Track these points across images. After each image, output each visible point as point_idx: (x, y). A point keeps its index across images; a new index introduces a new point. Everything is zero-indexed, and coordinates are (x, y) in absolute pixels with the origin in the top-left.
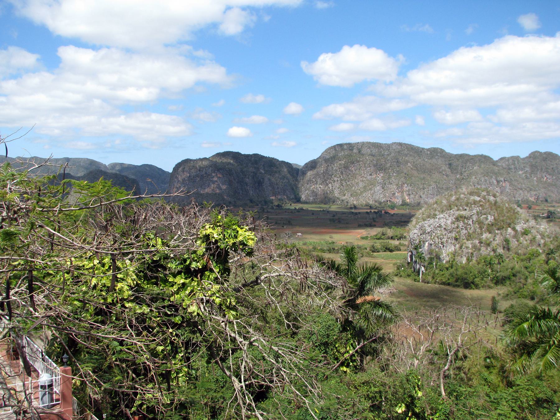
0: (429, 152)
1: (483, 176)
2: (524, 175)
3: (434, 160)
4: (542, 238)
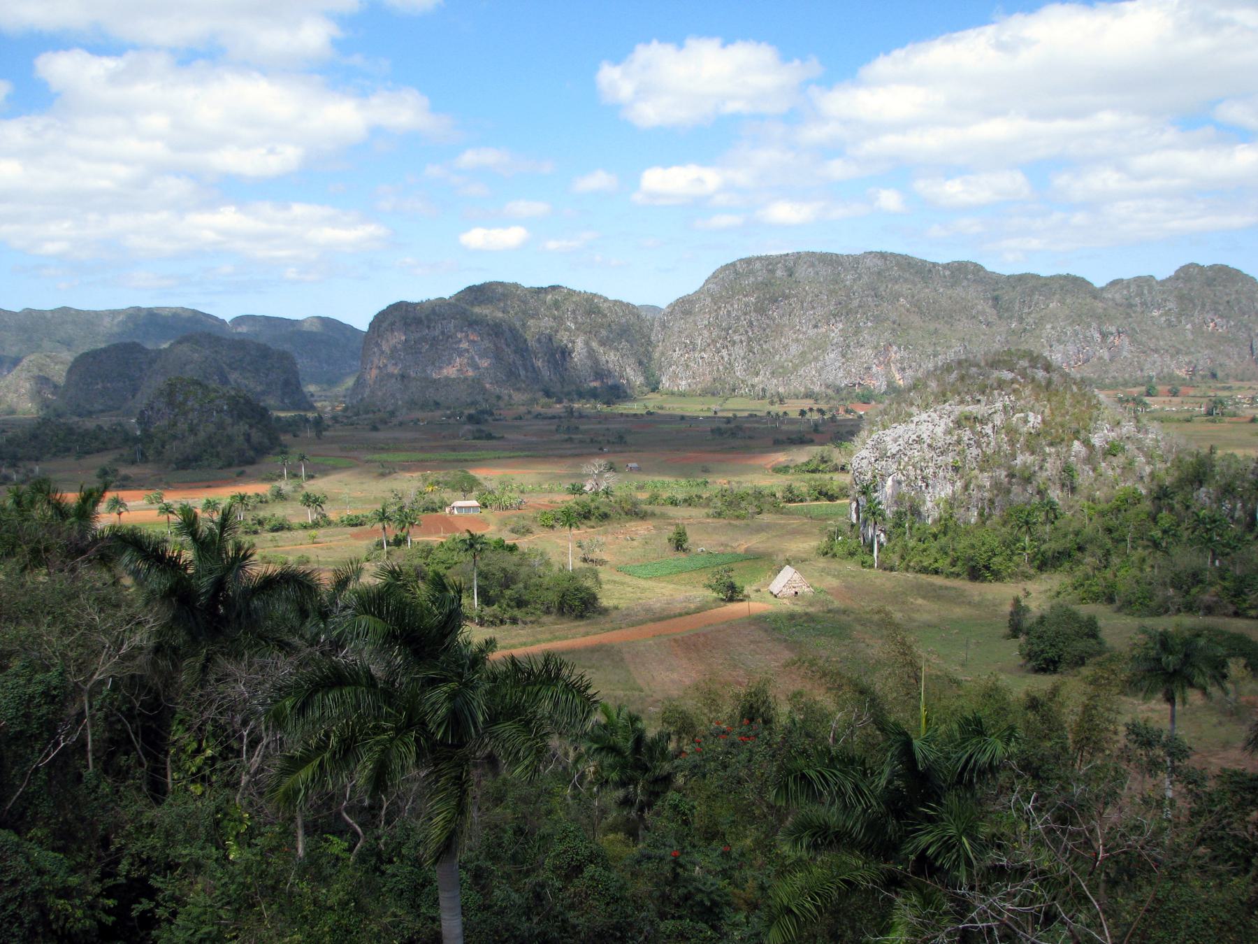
0: (947, 273)
1: (1070, 324)
2: (1163, 319)
4: (1148, 463)
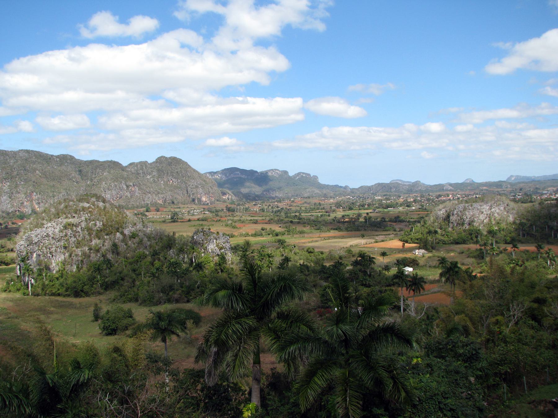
0: (58, 159)
2: (152, 179)
3: (64, 167)
4: (149, 241)
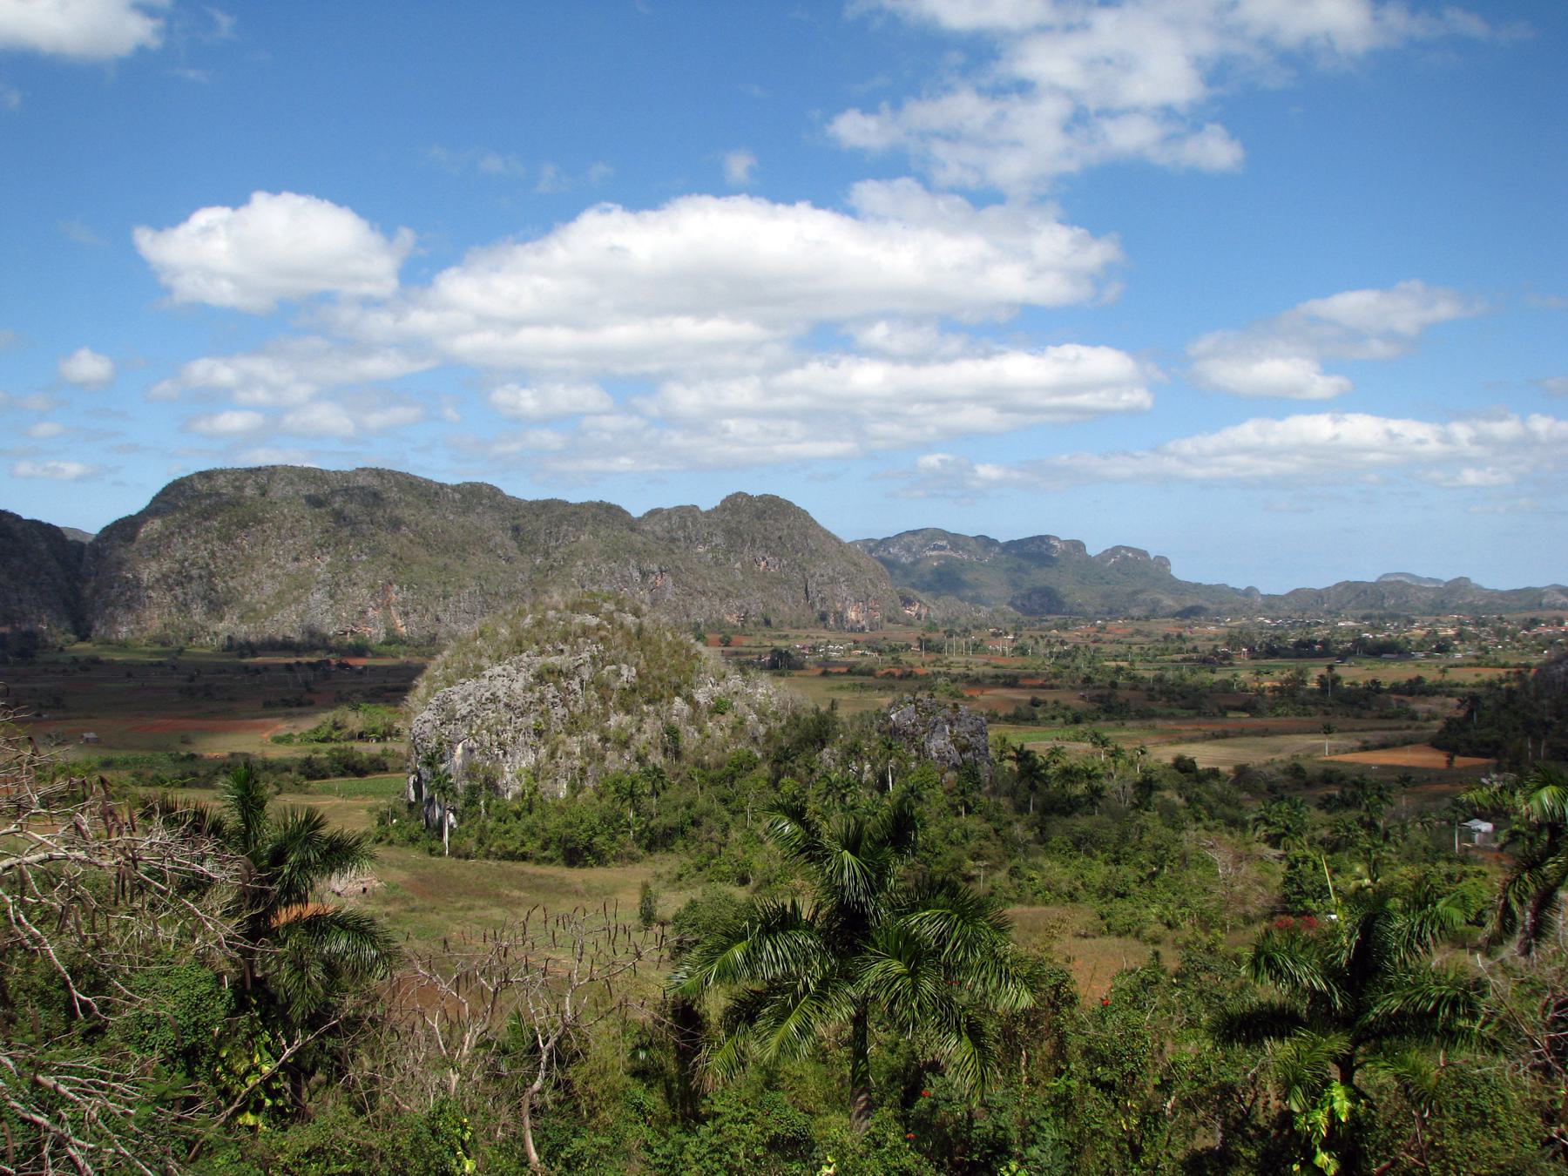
0: (457, 496)
3: (473, 517)
4: (761, 721)
